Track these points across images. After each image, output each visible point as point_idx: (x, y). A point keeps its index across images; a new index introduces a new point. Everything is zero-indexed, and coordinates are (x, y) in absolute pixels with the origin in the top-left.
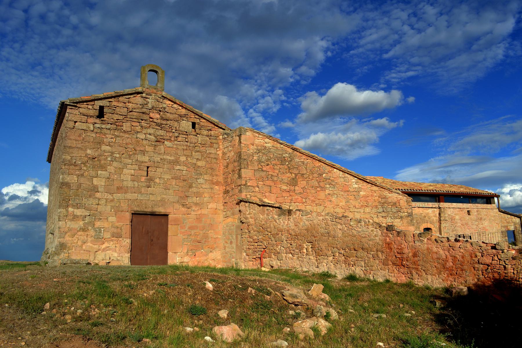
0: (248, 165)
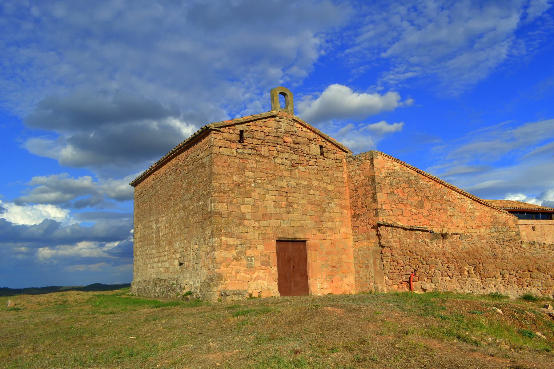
0: (381, 188)
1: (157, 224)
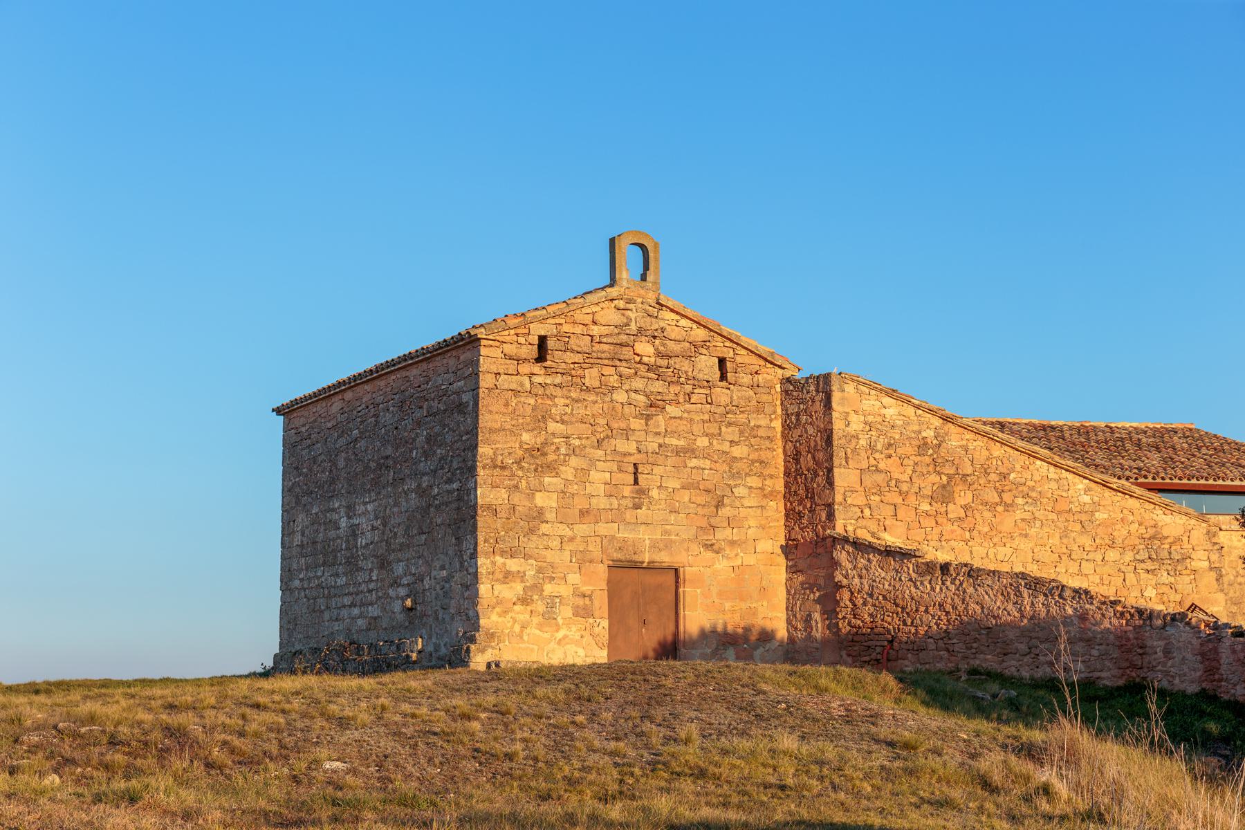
0: (847, 458)
1: (349, 518)
